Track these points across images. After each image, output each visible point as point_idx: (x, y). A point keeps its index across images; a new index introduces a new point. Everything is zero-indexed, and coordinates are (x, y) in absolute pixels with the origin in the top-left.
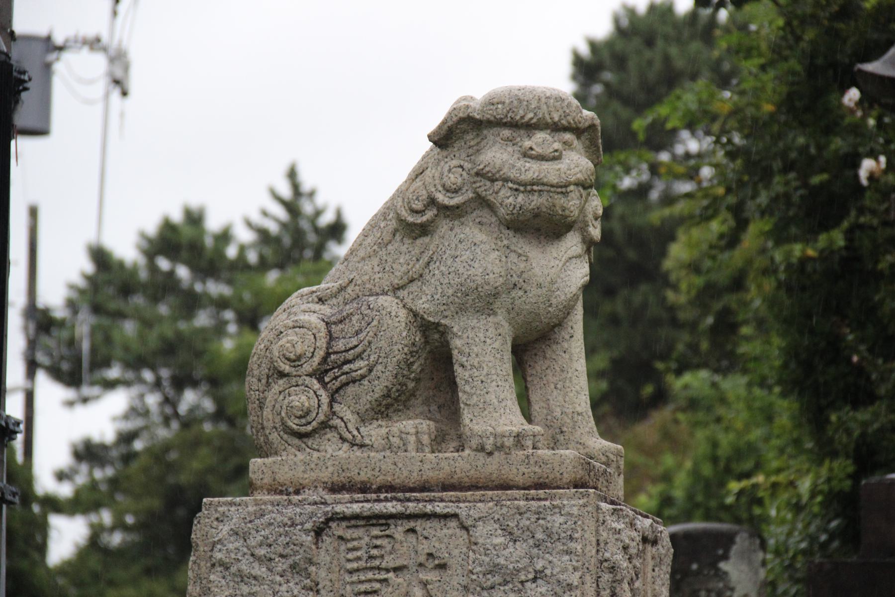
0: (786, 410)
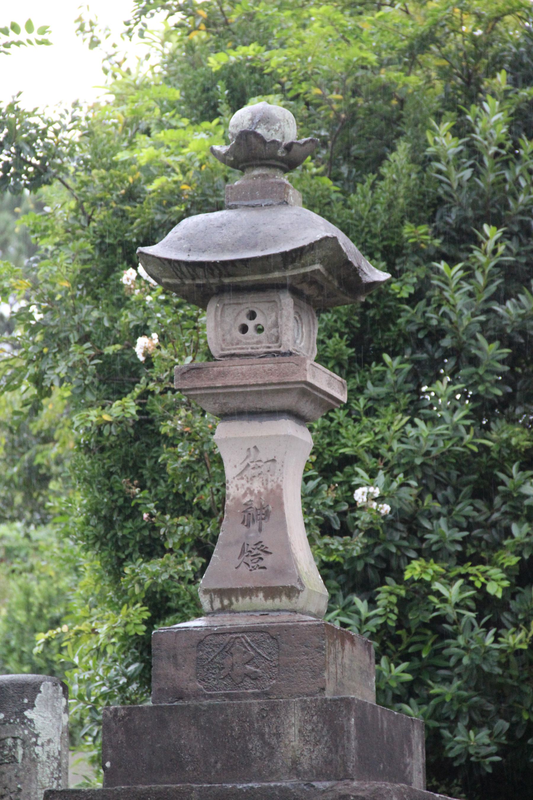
0: (90, 562)
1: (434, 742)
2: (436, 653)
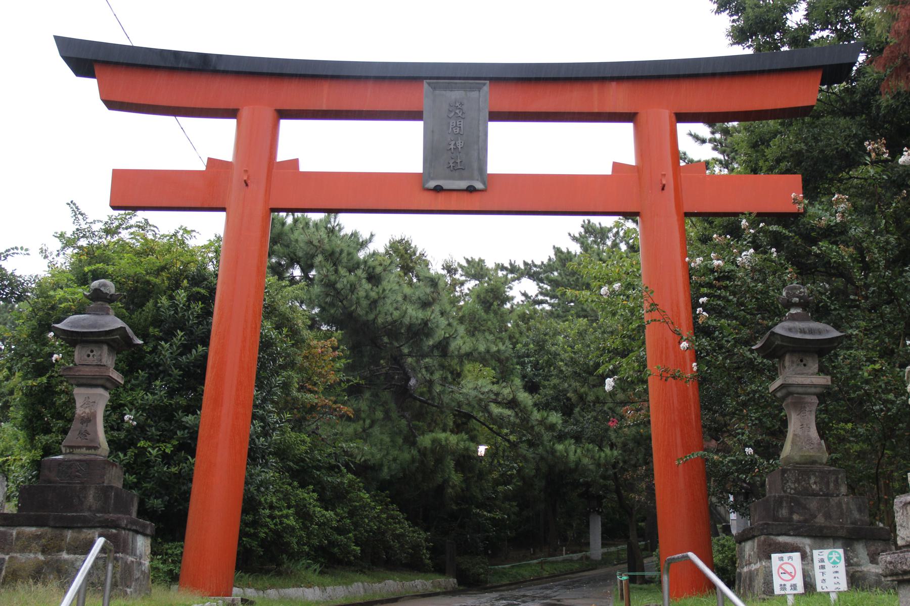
0: (21, 434)
1: (142, 503)
2: (146, 473)
